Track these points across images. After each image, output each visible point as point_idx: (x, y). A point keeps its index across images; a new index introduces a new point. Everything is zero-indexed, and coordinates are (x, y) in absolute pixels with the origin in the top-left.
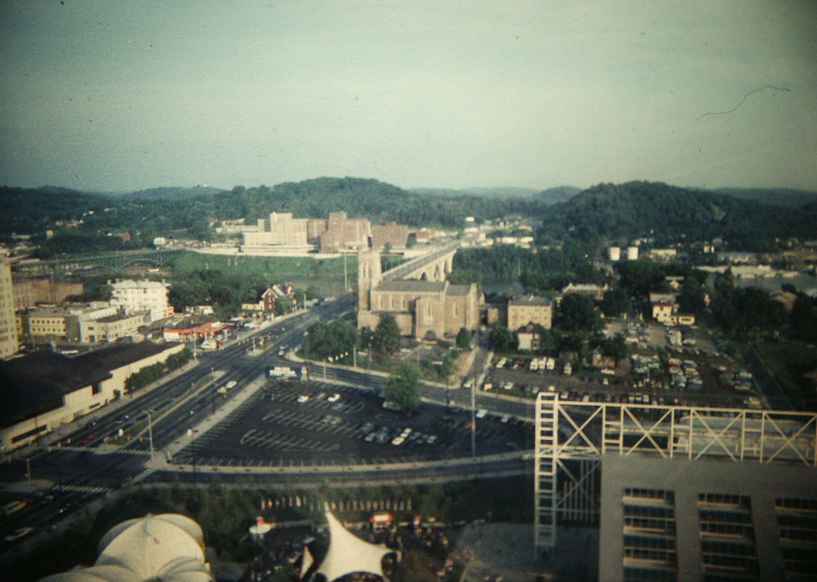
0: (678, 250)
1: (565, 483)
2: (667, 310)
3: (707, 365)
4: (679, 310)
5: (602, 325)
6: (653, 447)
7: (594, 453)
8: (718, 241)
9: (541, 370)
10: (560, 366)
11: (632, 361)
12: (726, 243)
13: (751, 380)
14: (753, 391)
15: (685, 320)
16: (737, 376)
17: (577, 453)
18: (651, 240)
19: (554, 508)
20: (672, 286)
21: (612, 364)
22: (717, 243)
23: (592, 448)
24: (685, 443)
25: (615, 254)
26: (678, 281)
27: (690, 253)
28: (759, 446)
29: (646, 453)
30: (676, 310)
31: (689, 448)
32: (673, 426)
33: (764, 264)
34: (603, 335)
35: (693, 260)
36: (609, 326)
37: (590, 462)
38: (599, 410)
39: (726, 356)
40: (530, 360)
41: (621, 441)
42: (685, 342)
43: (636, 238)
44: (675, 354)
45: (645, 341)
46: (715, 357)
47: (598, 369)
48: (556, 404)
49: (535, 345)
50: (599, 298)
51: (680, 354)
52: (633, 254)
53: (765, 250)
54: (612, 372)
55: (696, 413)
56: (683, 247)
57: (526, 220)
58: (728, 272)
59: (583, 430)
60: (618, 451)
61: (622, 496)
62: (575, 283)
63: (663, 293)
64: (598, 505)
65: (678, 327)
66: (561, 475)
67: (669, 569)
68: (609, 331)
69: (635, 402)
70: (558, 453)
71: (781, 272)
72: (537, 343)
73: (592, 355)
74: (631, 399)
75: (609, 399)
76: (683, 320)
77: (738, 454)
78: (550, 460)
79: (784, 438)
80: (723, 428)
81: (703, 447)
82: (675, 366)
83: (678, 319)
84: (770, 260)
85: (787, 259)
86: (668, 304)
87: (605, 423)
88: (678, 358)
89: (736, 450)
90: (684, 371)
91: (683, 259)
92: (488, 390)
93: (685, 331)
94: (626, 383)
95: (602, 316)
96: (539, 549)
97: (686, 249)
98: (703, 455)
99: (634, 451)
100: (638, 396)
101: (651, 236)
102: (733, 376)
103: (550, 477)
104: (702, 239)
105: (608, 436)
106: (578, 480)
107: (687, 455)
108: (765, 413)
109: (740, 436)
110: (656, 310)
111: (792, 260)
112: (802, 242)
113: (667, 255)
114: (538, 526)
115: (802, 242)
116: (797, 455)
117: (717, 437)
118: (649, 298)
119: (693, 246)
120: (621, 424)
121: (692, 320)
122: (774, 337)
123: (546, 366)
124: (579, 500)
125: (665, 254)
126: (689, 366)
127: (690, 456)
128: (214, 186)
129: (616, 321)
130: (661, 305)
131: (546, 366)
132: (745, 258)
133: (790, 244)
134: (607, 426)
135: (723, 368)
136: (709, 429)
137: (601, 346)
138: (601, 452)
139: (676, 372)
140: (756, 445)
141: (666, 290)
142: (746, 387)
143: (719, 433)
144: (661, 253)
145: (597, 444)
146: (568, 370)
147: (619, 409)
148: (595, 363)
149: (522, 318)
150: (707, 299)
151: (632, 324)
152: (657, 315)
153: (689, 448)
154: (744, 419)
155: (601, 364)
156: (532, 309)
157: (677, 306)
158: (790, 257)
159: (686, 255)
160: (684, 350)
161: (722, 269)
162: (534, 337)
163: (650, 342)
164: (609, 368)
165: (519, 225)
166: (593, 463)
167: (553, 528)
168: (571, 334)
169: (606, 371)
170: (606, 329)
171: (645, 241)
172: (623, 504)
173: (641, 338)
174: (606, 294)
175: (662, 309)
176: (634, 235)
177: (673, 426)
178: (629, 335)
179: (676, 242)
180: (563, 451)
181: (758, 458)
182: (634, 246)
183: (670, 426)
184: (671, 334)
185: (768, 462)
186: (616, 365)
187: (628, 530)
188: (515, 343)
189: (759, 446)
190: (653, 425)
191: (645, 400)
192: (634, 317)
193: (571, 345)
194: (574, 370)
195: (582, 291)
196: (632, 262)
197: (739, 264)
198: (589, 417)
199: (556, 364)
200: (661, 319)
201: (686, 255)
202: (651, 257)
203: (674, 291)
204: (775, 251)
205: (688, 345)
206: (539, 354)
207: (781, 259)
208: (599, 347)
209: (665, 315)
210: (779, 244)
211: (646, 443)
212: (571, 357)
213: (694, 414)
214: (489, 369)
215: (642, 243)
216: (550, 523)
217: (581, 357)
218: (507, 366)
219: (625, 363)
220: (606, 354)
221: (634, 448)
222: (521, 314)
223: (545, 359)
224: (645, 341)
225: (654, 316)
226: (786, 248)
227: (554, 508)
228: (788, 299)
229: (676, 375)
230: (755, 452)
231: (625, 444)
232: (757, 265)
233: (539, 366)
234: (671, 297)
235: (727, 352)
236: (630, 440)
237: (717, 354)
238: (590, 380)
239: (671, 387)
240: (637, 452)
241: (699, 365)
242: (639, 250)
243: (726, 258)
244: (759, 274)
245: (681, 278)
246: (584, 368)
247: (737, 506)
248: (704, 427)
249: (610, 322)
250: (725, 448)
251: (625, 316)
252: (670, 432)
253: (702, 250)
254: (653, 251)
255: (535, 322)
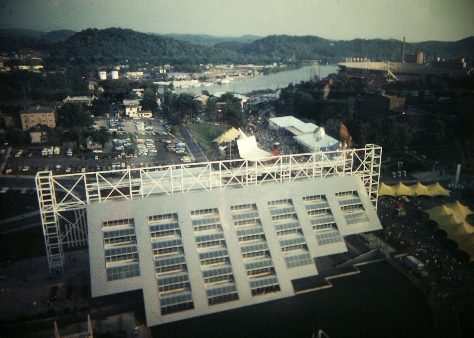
0: (144, 72)
1: (66, 226)
2: (135, 110)
3: (160, 141)
4: (142, 109)
5: (92, 122)
6: (120, 195)
7: (82, 204)
8: (167, 66)
9: (50, 155)
10: (64, 152)
11: (114, 143)
12: (172, 67)
13: (185, 147)
14: (186, 153)
15: (146, 115)
16: (177, 145)
17: (71, 206)
18: (127, 66)
19: (60, 242)
20: (137, 94)
21: (100, 146)
22: (167, 67)
23: (81, 202)
24: (179, 185)
25: (103, 76)
26: (142, 92)
27: (151, 74)
28: (181, 185)
29: (116, 199)
30: (140, 110)
31: (181, 187)
32: (130, 181)
33: (194, 79)
34: (93, 128)
35: (154, 78)
36: (98, 122)
37: (81, 210)
38: (82, 177)
39: (170, 134)
40: (42, 150)
41: (99, 194)
42: (146, 128)
43: (117, 65)
44: (141, 137)
45: (121, 130)
46: (164, 135)
47: (90, 151)
48: (51, 177)
49: (44, 139)
50: (90, 105)
51: (144, 135)
52: (115, 75)
53: (194, 71)
54: (101, 151)
55: (184, 167)
56: (147, 70)
57: (38, 53)
58: (171, 86)
59: (360, 163)
60: (98, 200)
61: (102, 227)
62: (72, 96)
63: (131, 99)
64: (86, 237)
65: (142, 119)
66: (62, 222)
67: (134, 263)
68: (97, 126)
69: (116, 168)
70: (56, 208)
71: (204, 83)
72: (45, 137)
73: (86, 142)
74: (114, 166)
75: (99, 169)
76: (145, 115)
77: (208, 187)
78: (52, 214)
79: (194, 178)
80: (160, 177)
81: (150, 190)
82: (141, 143)
83: (142, 115)
84: (198, 77)
85: (207, 75)
86: (135, 106)
87: (86, 185)
88: (143, 139)
89: (207, 185)
90: (146, 145)
91: (148, 77)
92: (9, 173)
93: (148, 122)
94: (110, 157)
95: (93, 116)
96: (52, 269)
97: (149, 71)
98: (150, 195)
99: (108, 199)
100: (118, 164)
101: (127, 64)
102: (175, 145)
103: (54, 224)
104: (157, 65)
105: (90, 193)
106: (74, 222)
107: (141, 195)
108: (291, 156)
109: (170, 180)
110: (128, 110)
111: (209, 76)
112: (214, 66)
113: (137, 75)
114: (50, 256)
115: (214, 66)
116: (202, 186)
117: (157, 183)
118: (122, 102)
119: (153, 69)
120: (97, 184)
121: (151, 115)
122: (198, 121)
123: (54, 152)
124: (77, 234)
125: (136, 74)
126: (149, 142)
127: (143, 196)
128: (252, 34)
129: (101, 119)
130: (131, 107)
131: (54, 152)
132: (183, 76)
133: (208, 67)
134: (88, 187)
135: (169, 142)
136: (152, 179)
137: (91, 136)
138: (86, 203)
139: (142, 147)
140: (180, 184)
141: (134, 97)
142: (182, 151)
143: (158, 181)
144: (134, 74)
145: (84, 198)
146: (70, 153)
147: (95, 175)
148: (89, 147)
149: (33, 121)
150: (159, 102)
151: (113, 120)
152: (129, 113)
153: (181, 187)
154: (171, 170)
155: (93, 147)
156: (40, 115)
157: (141, 107)
158: (208, 75)
159: (149, 75)
160: (146, 133)
161: (168, 83)
162: (42, 134)
163: (124, 130)
164: (99, 149)
165: (30, 57)
166: (83, 210)
167: (61, 255)
168: (69, 130)
169: (96, 151)
170: (95, 124)
171: (123, 67)
172: (192, 220)
173: (119, 128)
174: (94, 102)
175: (131, 109)
176: (116, 62)
177: (130, 181)
178: (110, 127)
179: (142, 67)
180: (61, 207)
181: (181, 191)
182: (116, 70)
183: (129, 180)
184: (138, 124)
185: (187, 192)
186: (103, 147)
187: (108, 246)
188: (29, 139)
189: (181, 185)
190: (118, 181)
191: (122, 166)
192: (114, 115)
193: (73, 137)
194: (74, 152)
195: (76, 101)
196: (116, 80)
197: (180, 80)
198: (77, 180)
199: (61, 150)
200: (131, 115)
201: (149, 75)
202: (128, 77)
203: (139, 98)
204: (200, 72)
205: (149, 130)
206: (48, 145)
207: (203, 76)
208: (89, 137)
209: (134, 113)
210: (202, 67)
211: (115, 193)
212: (72, 144)
213: (183, 168)
214: (9, 158)
215: (121, 68)
216: (58, 252)
217: (78, 144)
218: (23, 155)
219: (109, 144)
220: (95, 140)
221: (108, 197)
222: (31, 119)
223: (52, 148)
224: (121, 130)
225: (127, 114)
226: (206, 70)
227: (60, 242)
228: (203, 99)
229: (141, 148)
230: (180, 188)
231: (102, 196)
232: (191, 79)
233: (48, 152)
234: (136, 102)
235: (171, 132)
236: (105, 193)
237: (166, 134)
238: (86, 158)
239: (139, 156)
240: (111, 199)
241: (155, 141)
242: (119, 72)
243: (173, 76)
244: (192, 85)
245: (143, 90)
246: (81, 151)
247: (171, 219)
248: (149, 178)
249: (98, 120)
250: (201, 184)
251: (108, 115)
252: (129, 184)
253: (159, 72)
254: (128, 73)
255: (42, 123)
